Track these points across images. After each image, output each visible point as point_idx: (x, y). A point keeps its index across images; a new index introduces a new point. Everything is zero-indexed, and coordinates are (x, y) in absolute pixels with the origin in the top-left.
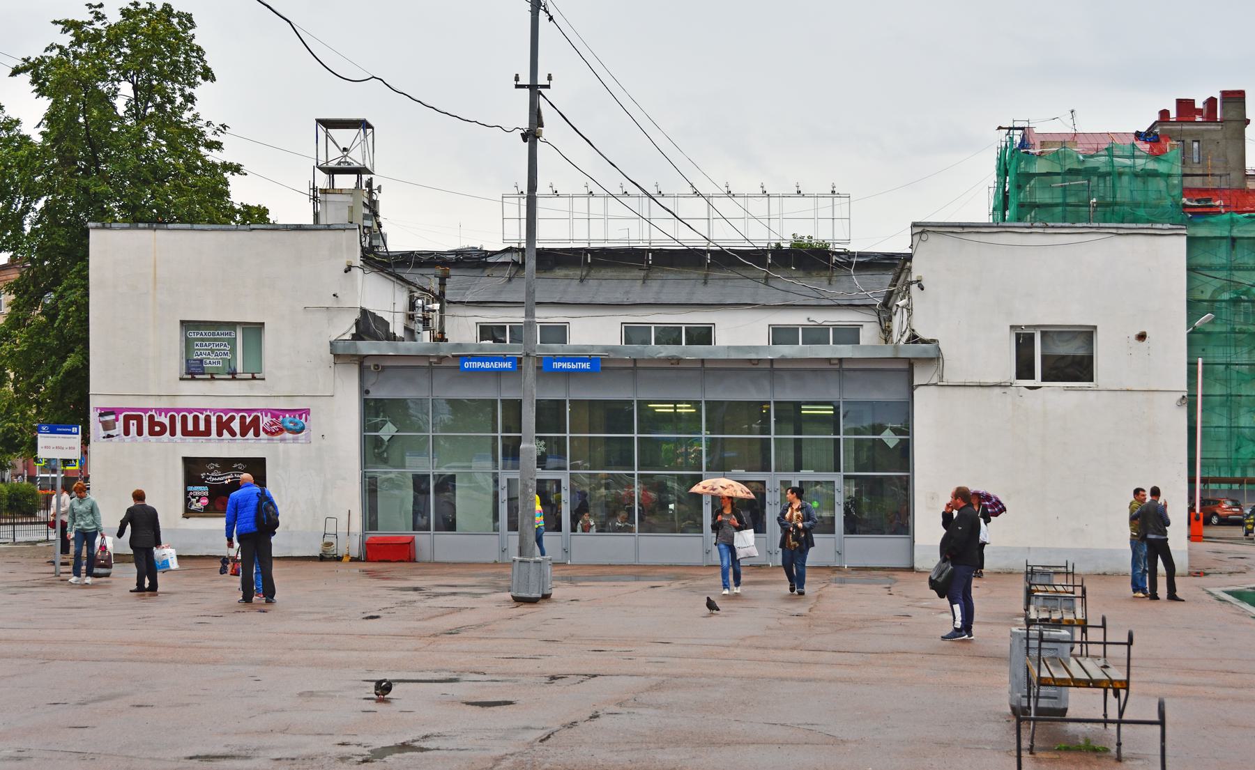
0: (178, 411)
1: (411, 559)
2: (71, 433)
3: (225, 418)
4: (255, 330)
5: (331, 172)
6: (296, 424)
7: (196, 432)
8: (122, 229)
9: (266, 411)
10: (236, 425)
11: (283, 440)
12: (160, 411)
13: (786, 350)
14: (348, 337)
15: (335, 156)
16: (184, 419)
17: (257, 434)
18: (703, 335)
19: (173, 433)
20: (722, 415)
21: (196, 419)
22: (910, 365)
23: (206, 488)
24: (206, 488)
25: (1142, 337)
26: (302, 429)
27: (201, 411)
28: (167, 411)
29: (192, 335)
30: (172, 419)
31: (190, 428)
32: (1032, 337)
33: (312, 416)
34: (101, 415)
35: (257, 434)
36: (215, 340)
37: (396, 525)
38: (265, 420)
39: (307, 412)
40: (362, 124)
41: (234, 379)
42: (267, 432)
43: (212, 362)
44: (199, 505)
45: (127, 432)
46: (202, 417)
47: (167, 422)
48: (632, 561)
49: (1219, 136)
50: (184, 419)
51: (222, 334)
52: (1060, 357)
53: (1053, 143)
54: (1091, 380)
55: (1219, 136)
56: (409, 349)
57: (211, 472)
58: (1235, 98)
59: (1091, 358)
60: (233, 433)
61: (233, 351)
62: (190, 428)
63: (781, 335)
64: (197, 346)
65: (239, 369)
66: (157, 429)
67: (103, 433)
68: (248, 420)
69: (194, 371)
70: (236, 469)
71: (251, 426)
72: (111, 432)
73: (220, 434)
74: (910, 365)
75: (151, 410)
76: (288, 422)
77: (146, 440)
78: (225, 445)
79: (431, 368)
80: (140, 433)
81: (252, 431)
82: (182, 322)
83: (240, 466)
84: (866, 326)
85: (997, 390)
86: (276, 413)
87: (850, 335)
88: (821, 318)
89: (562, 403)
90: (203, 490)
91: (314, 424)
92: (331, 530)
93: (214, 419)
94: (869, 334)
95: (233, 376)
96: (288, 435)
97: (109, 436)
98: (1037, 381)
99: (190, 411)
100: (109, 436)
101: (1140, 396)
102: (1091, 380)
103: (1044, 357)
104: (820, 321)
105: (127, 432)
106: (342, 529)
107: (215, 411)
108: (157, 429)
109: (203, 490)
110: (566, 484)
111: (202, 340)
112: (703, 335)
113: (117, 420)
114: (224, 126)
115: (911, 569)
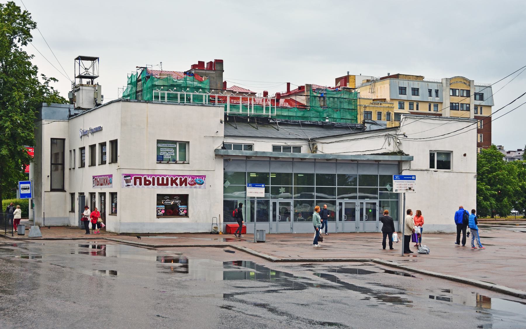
0: (156, 175)
3: (174, 179)
4: (184, 145)
5: (81, 77)
6: (200, 181)
7: (163, 184)
8: (135, 102)
9: (189, 176)
10: (178, 181)
12: (148, 175)
13: (276, 154)
14: (220, 148)
15: (83, 72)
16: (158, 179)
17: (186, 185)
18: (250, 147)
19: (154, 185)
21: (163, 179)
22: (400, 163)
23: (164, 206)
24: (164, 206)
25: (465, 155)
26: (203, 183)
27: (165, 176)
28: (151, 175)
29: (160, 145)
30: (154, 179)
31: (160, 182)
32: (434, 154)
34: (125, 177)
35: (186, 185)
38: (189, 180)
39: (205, 176)
40: (93, 59)
41: (176, 163)
42: (190, 184)
43: (167, 156)
44: (161, 213)
45: (135, 184)
46: (165, 178)
47: (151, 180)
49: (214, 76)
50: (158, 179)
52: (442, 161)
53: (164, 75)
54: (449, 168)
55: (214, 76)
56: (246, 153)
57: (166, 200)
58: (220, 62)
59: (449, 162)
60: (177, 185)
61: (175, 152)
62: (160, 182)
63: (276, 148)
64: (161, 150)
65: (178, 159)
66: (147, 183)
67: (126, 184)
68: (183, 179)
69: (160, 159)
70: (176, 199)
71: (184, 182)
72: (129, 184)
73: (172, 185)
74: (400, 163)
76: (198, 180)
77: (143, 187)
78: (177, 189)
79: (358, 164)
80: (141, 184)
81: (184, 184)
83: (177, 198)
84: (304, 146)
85: (426, 172)
86: (193, 177)
87: (298, 149)
88: (290, 143)
89: (313, 175)
90: (163, 207)
91: (207, 181)
92: (215, 222)
93: (170, 179)
94: (305, 150)
96: (197, 185)
97: (128, 185)
98: (435, 169)
99: (160, 176)
100: (128, 185)
101: (464, 174)
102: (449, 168)
103: (437, 161)
104: (289, 144)
105: (135, 184)
106: (218, 222)
107: (170, 176)
108: (147, 183)
109: (163, 207)
112: (250, 147)
113: (131, 179)
114: (33, 55)
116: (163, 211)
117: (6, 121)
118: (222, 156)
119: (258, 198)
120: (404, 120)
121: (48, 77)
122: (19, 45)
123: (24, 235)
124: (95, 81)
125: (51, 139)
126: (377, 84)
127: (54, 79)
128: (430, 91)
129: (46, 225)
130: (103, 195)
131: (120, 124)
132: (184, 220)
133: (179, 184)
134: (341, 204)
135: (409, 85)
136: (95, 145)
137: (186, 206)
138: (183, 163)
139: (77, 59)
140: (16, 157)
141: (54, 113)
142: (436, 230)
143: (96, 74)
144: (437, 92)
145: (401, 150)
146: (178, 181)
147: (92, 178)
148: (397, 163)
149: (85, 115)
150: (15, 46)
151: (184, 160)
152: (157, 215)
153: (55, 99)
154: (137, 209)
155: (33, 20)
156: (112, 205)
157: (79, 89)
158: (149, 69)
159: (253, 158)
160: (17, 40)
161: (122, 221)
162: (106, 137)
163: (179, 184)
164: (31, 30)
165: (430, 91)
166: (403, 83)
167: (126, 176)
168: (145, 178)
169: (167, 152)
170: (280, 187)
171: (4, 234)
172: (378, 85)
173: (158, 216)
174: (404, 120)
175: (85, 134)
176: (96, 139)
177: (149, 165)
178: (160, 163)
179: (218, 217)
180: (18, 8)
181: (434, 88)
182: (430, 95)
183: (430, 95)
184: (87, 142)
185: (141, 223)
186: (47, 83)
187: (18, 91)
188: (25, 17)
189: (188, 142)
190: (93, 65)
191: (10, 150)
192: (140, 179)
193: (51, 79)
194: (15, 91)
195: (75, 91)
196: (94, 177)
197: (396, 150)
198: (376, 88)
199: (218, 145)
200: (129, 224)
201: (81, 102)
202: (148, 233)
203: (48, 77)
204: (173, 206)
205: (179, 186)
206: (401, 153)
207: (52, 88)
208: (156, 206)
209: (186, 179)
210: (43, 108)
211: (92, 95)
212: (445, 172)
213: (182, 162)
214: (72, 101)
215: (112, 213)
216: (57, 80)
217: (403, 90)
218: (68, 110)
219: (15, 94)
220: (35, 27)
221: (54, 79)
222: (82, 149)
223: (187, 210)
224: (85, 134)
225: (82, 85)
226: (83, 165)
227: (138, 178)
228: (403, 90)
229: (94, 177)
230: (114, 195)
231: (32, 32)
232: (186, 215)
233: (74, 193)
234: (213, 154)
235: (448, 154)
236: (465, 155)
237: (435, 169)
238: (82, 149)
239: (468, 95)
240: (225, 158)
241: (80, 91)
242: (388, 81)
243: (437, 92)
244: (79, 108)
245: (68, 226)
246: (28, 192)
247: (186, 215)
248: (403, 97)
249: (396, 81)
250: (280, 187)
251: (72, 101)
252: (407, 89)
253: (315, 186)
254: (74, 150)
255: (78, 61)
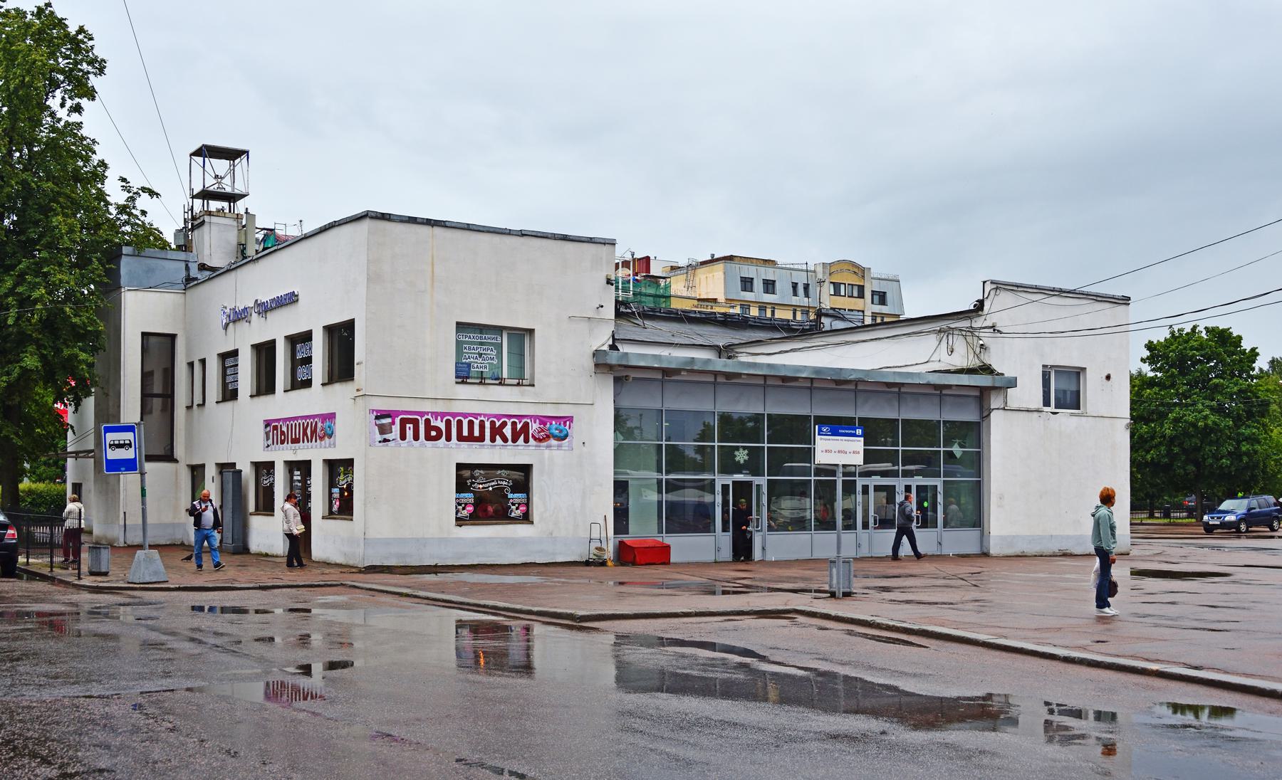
0: (454, 415)
1: (666, 562)
2: (854, 435)
3: (498, 424)
4: (522, 336)
6: (561, 431)
7: (471, 438)
9: (534, 418)
10: (508, 431)
11: (549, 447)
12: (436, 415)
14: (606, 348)
16: (460, 423)
17: (526, 441)
19: (449, 439)
20: (733, 427)
21: (471, 424)
22: (983, 394)
24: (471, 495)
25: (1108, 377)
26: (566, 436)
27: (476, 416)
28: (443, 415)
30: (448, 423)
31: (465, 433)
33: (574, 425)
35: (526, 441)
36: (481, 344)
37: (643, 529)
38: (534, 427)
39: (571, 419)
41: (500, 384)
42: (535, 439)
43: (478, 365)
44: (465, 513)
45: (403, 437)
46: (477, 422)
47: (442, 426)
48: (808, 556)
50: (460, 423)
51: (488, 338)
52: (1065, 389)
60: (505, 440)
62: (465, 433)
65: (505, 375)
66: (433, 435)
67: (379, 437)
68: (519, 426)
69: (463, 376)
71: (521, 433)
72: (387, 436)
73: (493, 440)
74: (983, 394)
75: (427, 413)
76: (553, 429)
77: (422, 445)
80: (416, 437)
81: (522, 437)
82: (458, 323)
85: (1036, 414)
86: (543, 420)
91: (576, 430)
92: (595, 535)
93: (487, 425)
95: (502, 383)
96: (553, 442)
97: (385, 440)
98: (1052, 408)
99: (465, 415)
100: (385, 440)
105: (403, 437)
106: (603, 535)
107: (489, 416)
108: (433, 433)
110: (940, 489)
111: (472, 343)
113: (393, 423)
115: (985, 555)
116: (471, 508)
117: (34, 286)
118: (610, 368)
119: (844, 466)
120: (993, 293)
121: (136, 184)
122: (62, 114)
123: (106, 574)
124: (240, 206)
125: (144, 334)
126: (699, 271)
127: (152, 193)
128: (795, 286)
129: (129, 542)
130: (305, 467)
131: (362, 279)
132: (520, 530)
133: (509, 437)
134: (865, 489)
135: (759, 275)
136: (272, 344)
137: (524, 495)
138: (518, 384)
139: (198, 153)
140: (59, 378)
141: (150, 271)
142: (1054, 547)
143: (239, 188)
144: (806, 287)
145: (987, 362)
146: (508, 431)
147: (262, 426)
148: (977, 393)
149: (239, 271)
150: (53, 115)
151: (521, 379)
152: (457, 519)
153: (148, 239)
154: (408, 504)
155: (99, 52)
156: (331, 494)
157: (203, 223)
158: (278, 232)
159: (684, 376)
160: (58, 100)
161: (372, 534)
162: (313, 317)
163: (509, 437)
164: (91, 76)
165: (795, 286)
166: (749, 271)
167: (381, 415)
168: (427, 421)
169: (480, 355)
170: (737, 448)
171: (46, 571)
172: (702, 273)
173: (460, 521)
174: (993, 293)
175: (238, 317)
176: (278, 328)
177: (438, 390)
178: (463, 382)
179: (602, 523)
180: (61, 23)
181: (801, 279)
182: (795, 294)
183: (795, 294)
184: (259, 330)
185: (418, 540)
186: (132, 199)
187: (65, 215)
188: (78, 43)
189: (531, 332)
190: (232, 171)
191: (43, 358)
192: (415, 423)
193: (144, 189)
194: (57, 215)
195: (192, 229)
196: (267, 423)
197: (974, 363)
198: (697, 279)
199: (601, 339)
200: (387, 542)
201: (206, 252)
202: (436, 566)
203: (136, 184)
204: (494, 497)
205: (510, 442)
206: (986, 369)
207: (144, 213)
208: (454, 495)
209: (526, 425)
210: (124, 261)
211: (232, 237)
212: (1072, 415)
213: (515, 382)
214: (185, 247)
215: (331, 512)
216: (157, 195)
217: (747, 284)
218: (183, 265)
219: (57, 220)
220: (101, 71)
221: (152, 193)
222: (229, 357)
223: (527, 505)
224: (238, 317)
225: (210, 213)
226: (229, 394)
227: (410, 421)
228: (747, 284)
229: (267, 423)
230: (339, 468)
231: (93, 81)
232: (526, 518)
233: (203, 466)
234: (590, 363)
235: (1077, 373)
236: (1108, 377)
237: (1052, 408)
238: (229, 357)
239: (861, 295)
240: (618, 374)
241: (206, 228)
242: (720, 267)
243: (806, 287)
244: (203, 267)
245: (182, 544)
246: (128, 454)
247: (526, 518)
248: (748, 296)
249: (733, 266)
250: (737, 448)
251: (185, 247)
252: (755, 282)
253: (766, 445)
254: (203, 362)
255: (200, 159)
